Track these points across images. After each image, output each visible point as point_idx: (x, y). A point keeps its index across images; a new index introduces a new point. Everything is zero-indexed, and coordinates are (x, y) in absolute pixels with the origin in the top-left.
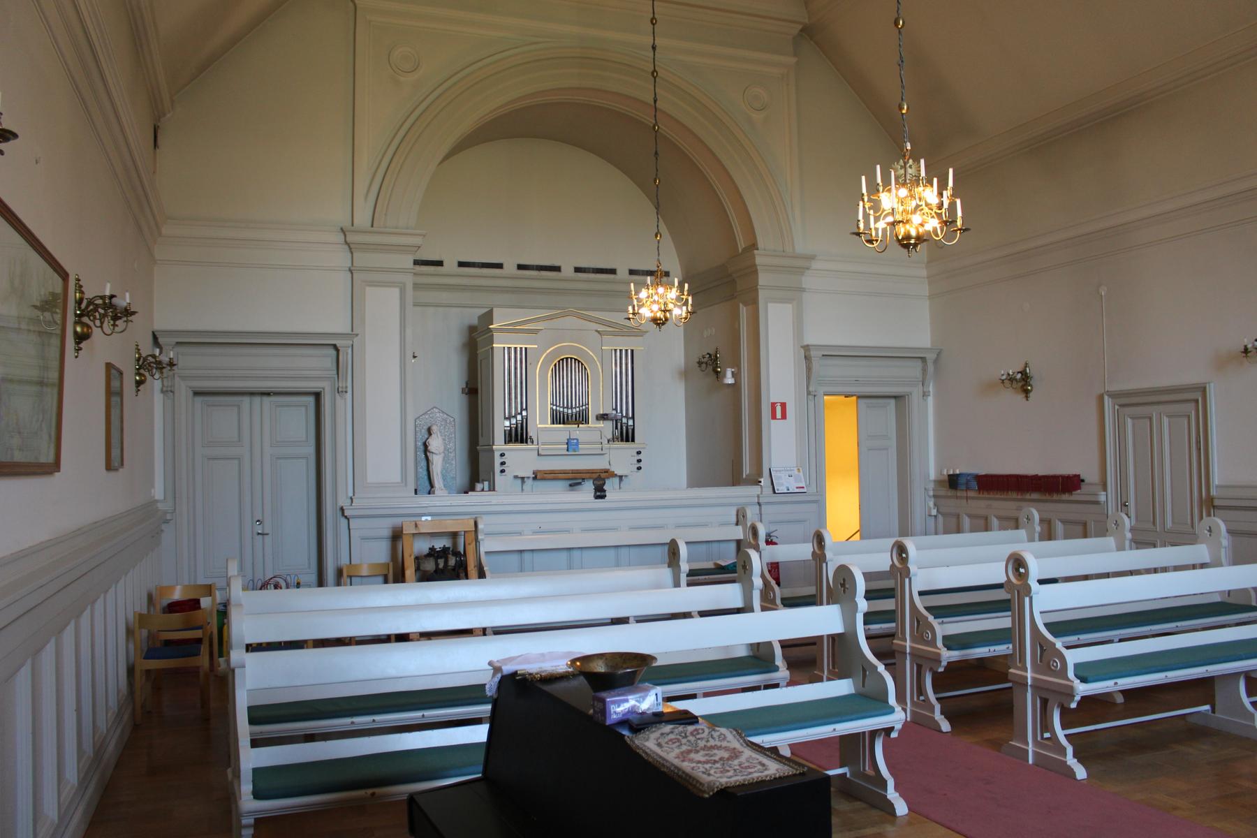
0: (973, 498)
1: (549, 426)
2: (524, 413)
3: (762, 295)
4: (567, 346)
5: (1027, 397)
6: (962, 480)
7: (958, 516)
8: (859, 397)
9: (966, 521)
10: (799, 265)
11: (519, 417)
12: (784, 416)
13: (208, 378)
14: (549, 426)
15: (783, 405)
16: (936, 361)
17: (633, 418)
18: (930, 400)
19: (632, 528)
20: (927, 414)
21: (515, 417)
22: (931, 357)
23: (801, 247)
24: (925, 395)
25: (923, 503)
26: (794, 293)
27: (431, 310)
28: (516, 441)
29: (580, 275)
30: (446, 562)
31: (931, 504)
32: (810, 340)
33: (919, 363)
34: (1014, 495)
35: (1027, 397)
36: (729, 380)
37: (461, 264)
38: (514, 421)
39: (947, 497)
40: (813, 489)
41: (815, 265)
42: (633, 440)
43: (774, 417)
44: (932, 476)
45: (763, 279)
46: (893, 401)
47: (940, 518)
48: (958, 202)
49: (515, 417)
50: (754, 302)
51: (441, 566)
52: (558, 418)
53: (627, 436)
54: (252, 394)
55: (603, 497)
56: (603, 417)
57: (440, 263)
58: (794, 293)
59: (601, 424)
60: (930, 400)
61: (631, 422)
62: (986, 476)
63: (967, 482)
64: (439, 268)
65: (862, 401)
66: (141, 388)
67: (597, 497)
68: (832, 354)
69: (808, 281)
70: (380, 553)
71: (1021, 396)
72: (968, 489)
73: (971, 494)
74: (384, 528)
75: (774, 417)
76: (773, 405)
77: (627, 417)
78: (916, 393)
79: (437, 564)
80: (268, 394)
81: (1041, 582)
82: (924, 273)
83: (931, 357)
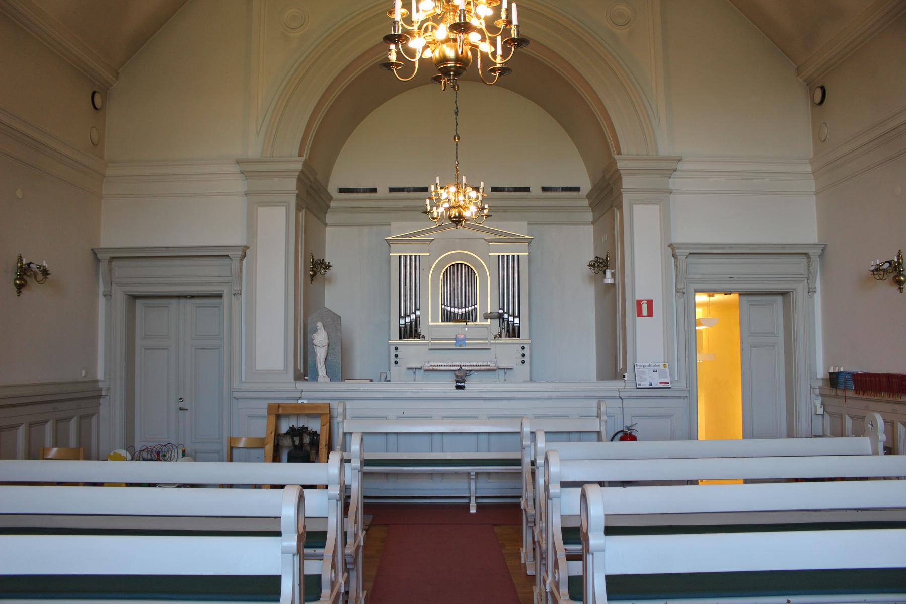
0: (851, 398)
1: (440, 323)
2: (418, 313)
3: (626, 198)
4: (457, 254)
5: (901, 289)
6: (841, 379)
7: (841, 416)
8: (740, 295)
9: (849, 423)
10: (668, 167)
11: (413, 316)
12: (650, 313)
13: (183, 284)
14: (440, 323)
15: (650, 303)
16: (822, 256)
17: (519, 316)
18: (818, 298)
19: (582, 417)
20: (815, 310)
21: (415, 313)
22: (815, 252)
23: (665, 149)
24: (811, 291)
25: (811, 403)
26: (661, 196)
27: (366, 229)
28: (410, 336)
29: (495, 193)
30: (301, 440)
31: (818, 402)
32: (677, 238)
33: (804, 259)
34: (886, 397)
35: (901, 289)
36: (609, 280)
37: (392, 190)
38: (408, 320)
39: (830, 396)
40: (682, 384)
41: (681, 166)
42: (519, 337)
43: (640, 314)
44: (821, 372)
45: (627, 182)
46: (779, 299)
47: (827, 416)
48: (514, 5)
49: (409, 316)
50: (620, 207)
51: (297, 443)
52: (447, 316)
53: (514, 332)
54: (179, 297)
55: (463, 387)
56: (486, 317)
57: (374, 190)
58: (661, 196)
59: (489, 322)
60: (818, 298)
61: (517, 320)
62: (865, 375)
63: (846, 381)
64: (373, 195)
65: (745, 298)
66: (23, 291)
67: (458, 387)
68: (698, 252)
69: (674, 183)
70: (261, 428)
71: (895, 288)
72: (845, 388)
73: (850, 393)
74: (262, 408)
75: (640, 314)
76: (639, 303)
77: (508, 312)
78: (800, 291)
79: (294, 442)
80: (192, 297)
81: (610, 530)
82: (809, 169)
83: (815, 252)
